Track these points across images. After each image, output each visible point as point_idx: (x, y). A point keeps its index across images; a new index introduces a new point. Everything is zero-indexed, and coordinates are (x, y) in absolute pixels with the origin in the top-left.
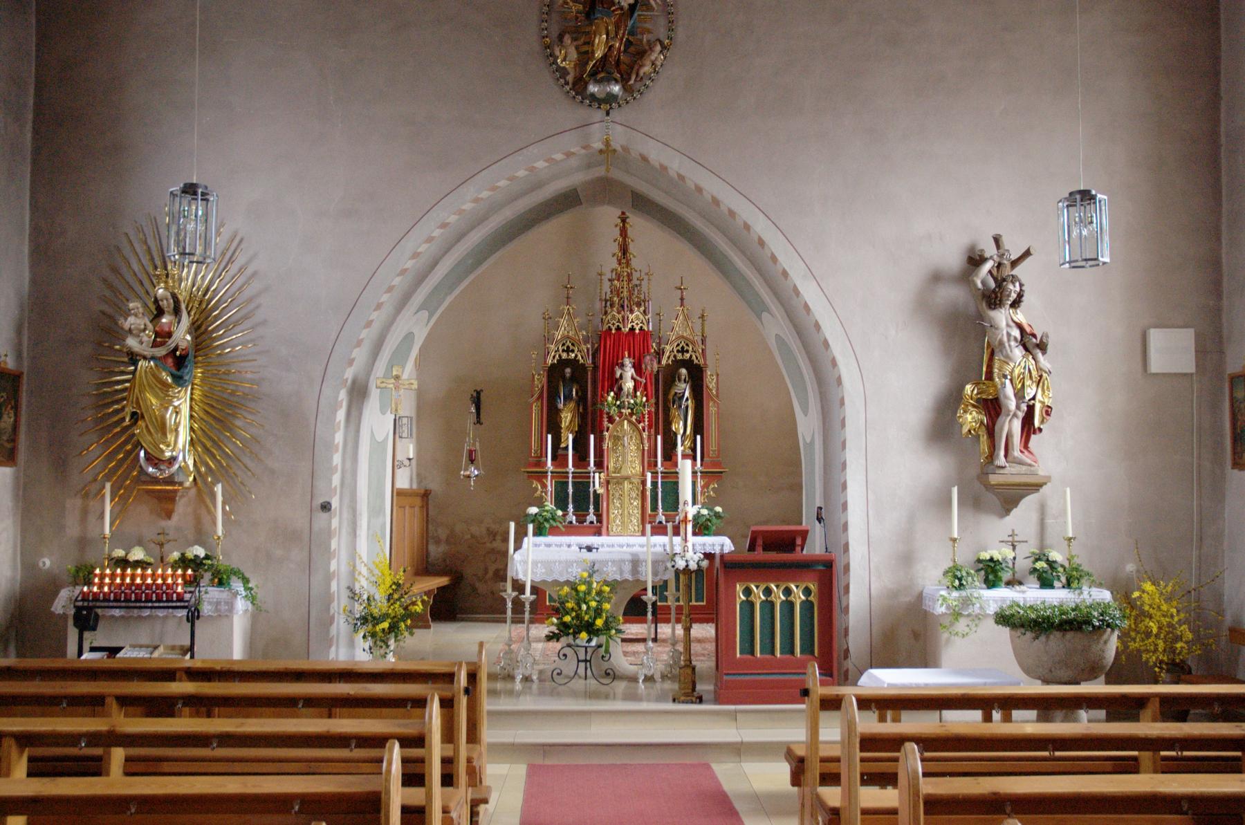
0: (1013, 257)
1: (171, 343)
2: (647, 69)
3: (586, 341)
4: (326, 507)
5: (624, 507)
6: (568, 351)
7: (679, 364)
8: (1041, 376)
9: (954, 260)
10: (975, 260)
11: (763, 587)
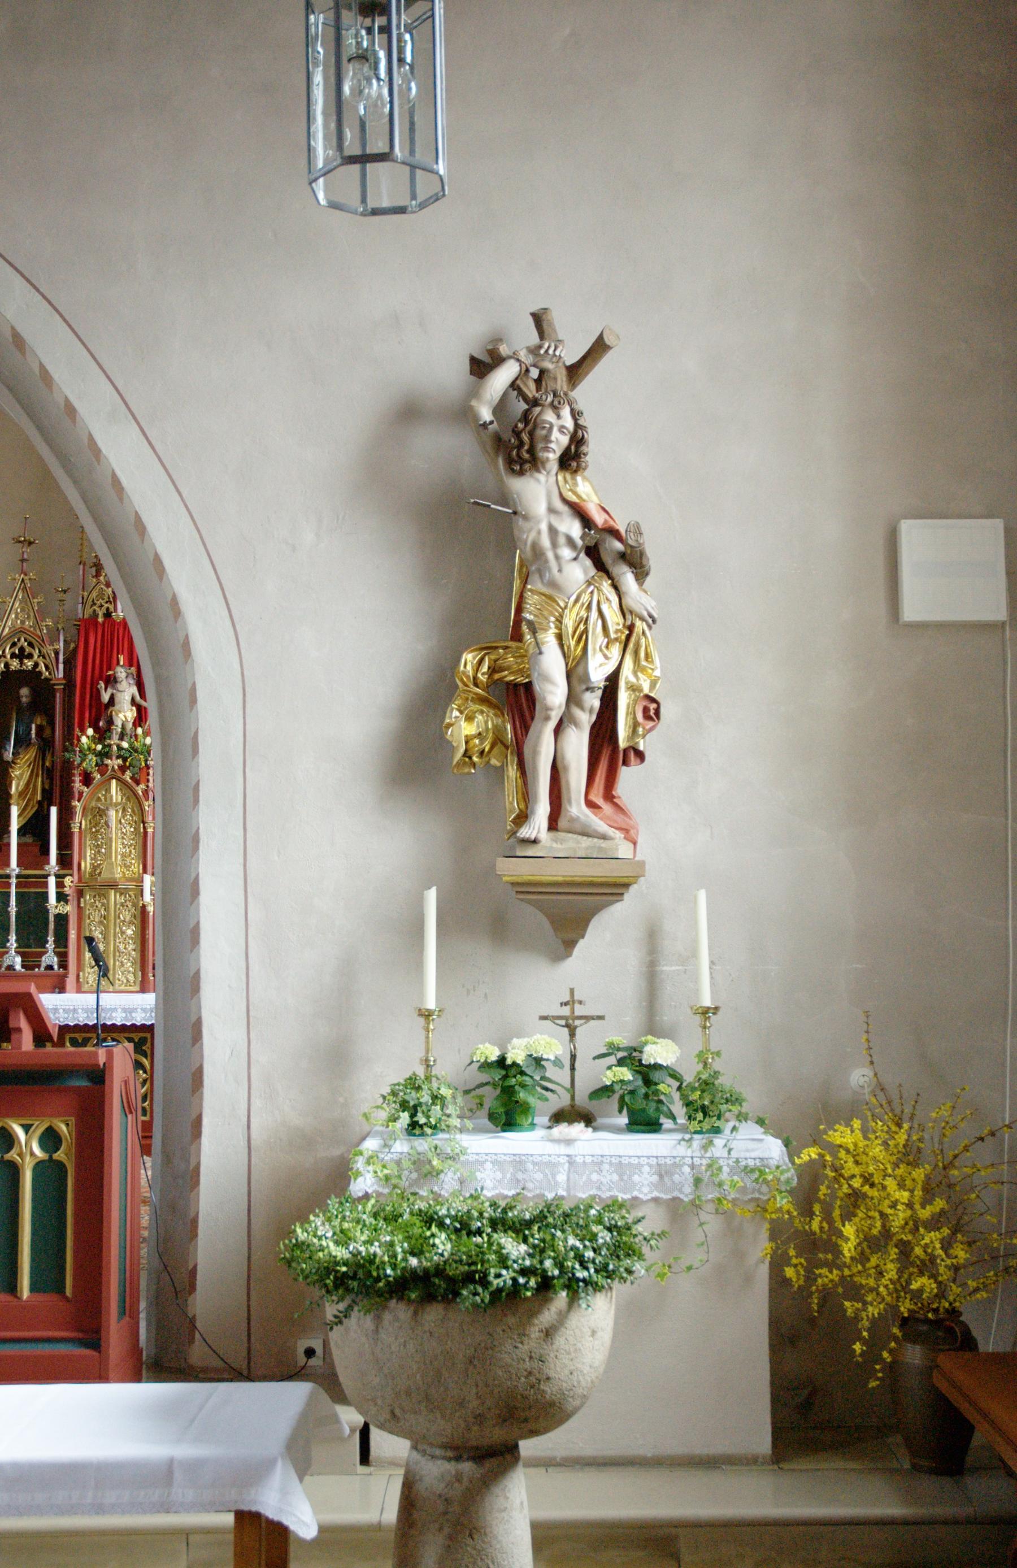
0: (571, 359)
6: (22, 656)
8: (631, 628)
11: (40, 1127)
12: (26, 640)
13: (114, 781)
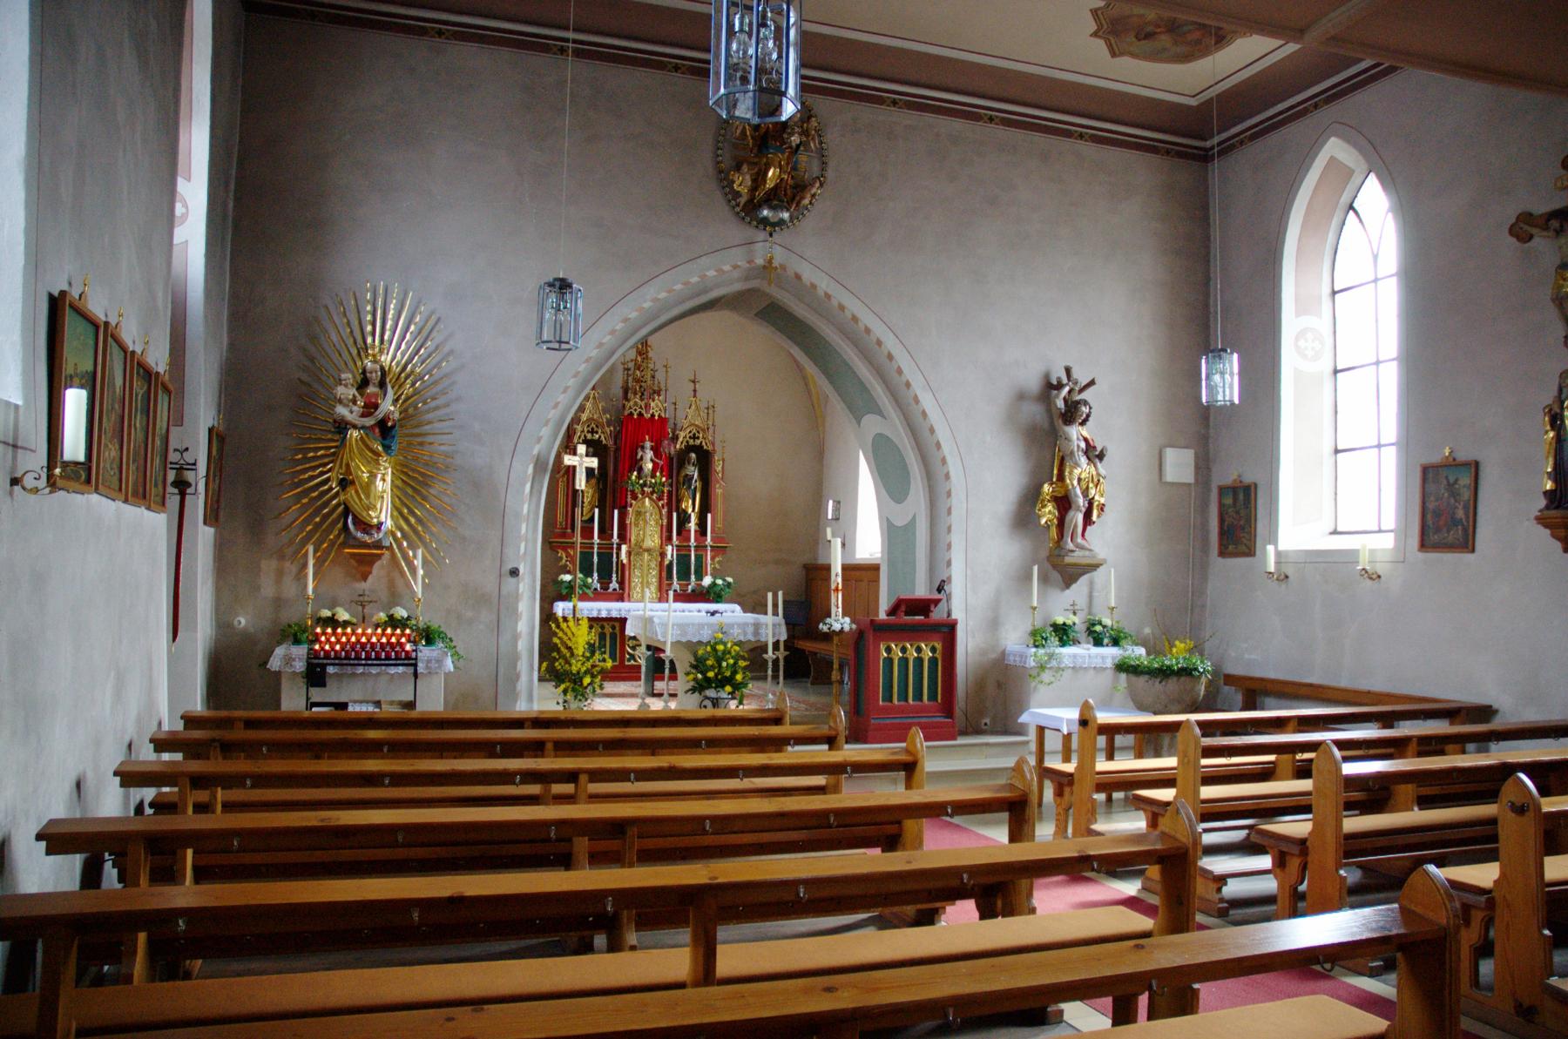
1: (380, 414)
2: (806, 202)
3: (609, 423)
4: (514, 573)
5: (644, 578)
6: (592, 432)
7: (690, 449)
9: (1033, 383)
10: (1051, 387)
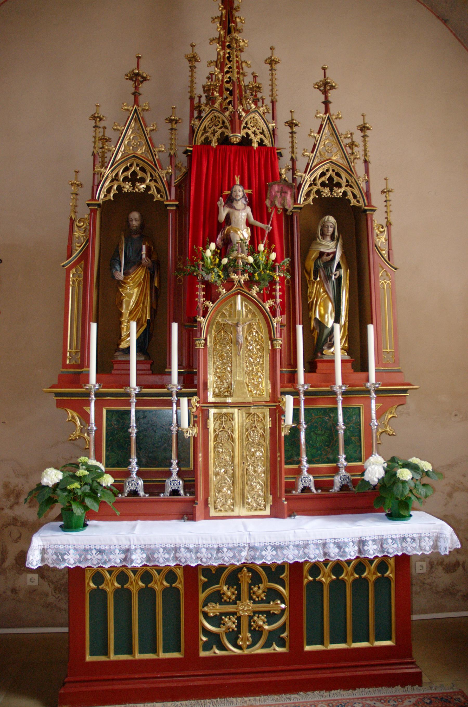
6: (134, 179)
12: (138, 165)
13: (239, 296)
